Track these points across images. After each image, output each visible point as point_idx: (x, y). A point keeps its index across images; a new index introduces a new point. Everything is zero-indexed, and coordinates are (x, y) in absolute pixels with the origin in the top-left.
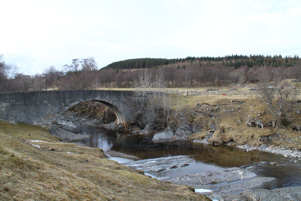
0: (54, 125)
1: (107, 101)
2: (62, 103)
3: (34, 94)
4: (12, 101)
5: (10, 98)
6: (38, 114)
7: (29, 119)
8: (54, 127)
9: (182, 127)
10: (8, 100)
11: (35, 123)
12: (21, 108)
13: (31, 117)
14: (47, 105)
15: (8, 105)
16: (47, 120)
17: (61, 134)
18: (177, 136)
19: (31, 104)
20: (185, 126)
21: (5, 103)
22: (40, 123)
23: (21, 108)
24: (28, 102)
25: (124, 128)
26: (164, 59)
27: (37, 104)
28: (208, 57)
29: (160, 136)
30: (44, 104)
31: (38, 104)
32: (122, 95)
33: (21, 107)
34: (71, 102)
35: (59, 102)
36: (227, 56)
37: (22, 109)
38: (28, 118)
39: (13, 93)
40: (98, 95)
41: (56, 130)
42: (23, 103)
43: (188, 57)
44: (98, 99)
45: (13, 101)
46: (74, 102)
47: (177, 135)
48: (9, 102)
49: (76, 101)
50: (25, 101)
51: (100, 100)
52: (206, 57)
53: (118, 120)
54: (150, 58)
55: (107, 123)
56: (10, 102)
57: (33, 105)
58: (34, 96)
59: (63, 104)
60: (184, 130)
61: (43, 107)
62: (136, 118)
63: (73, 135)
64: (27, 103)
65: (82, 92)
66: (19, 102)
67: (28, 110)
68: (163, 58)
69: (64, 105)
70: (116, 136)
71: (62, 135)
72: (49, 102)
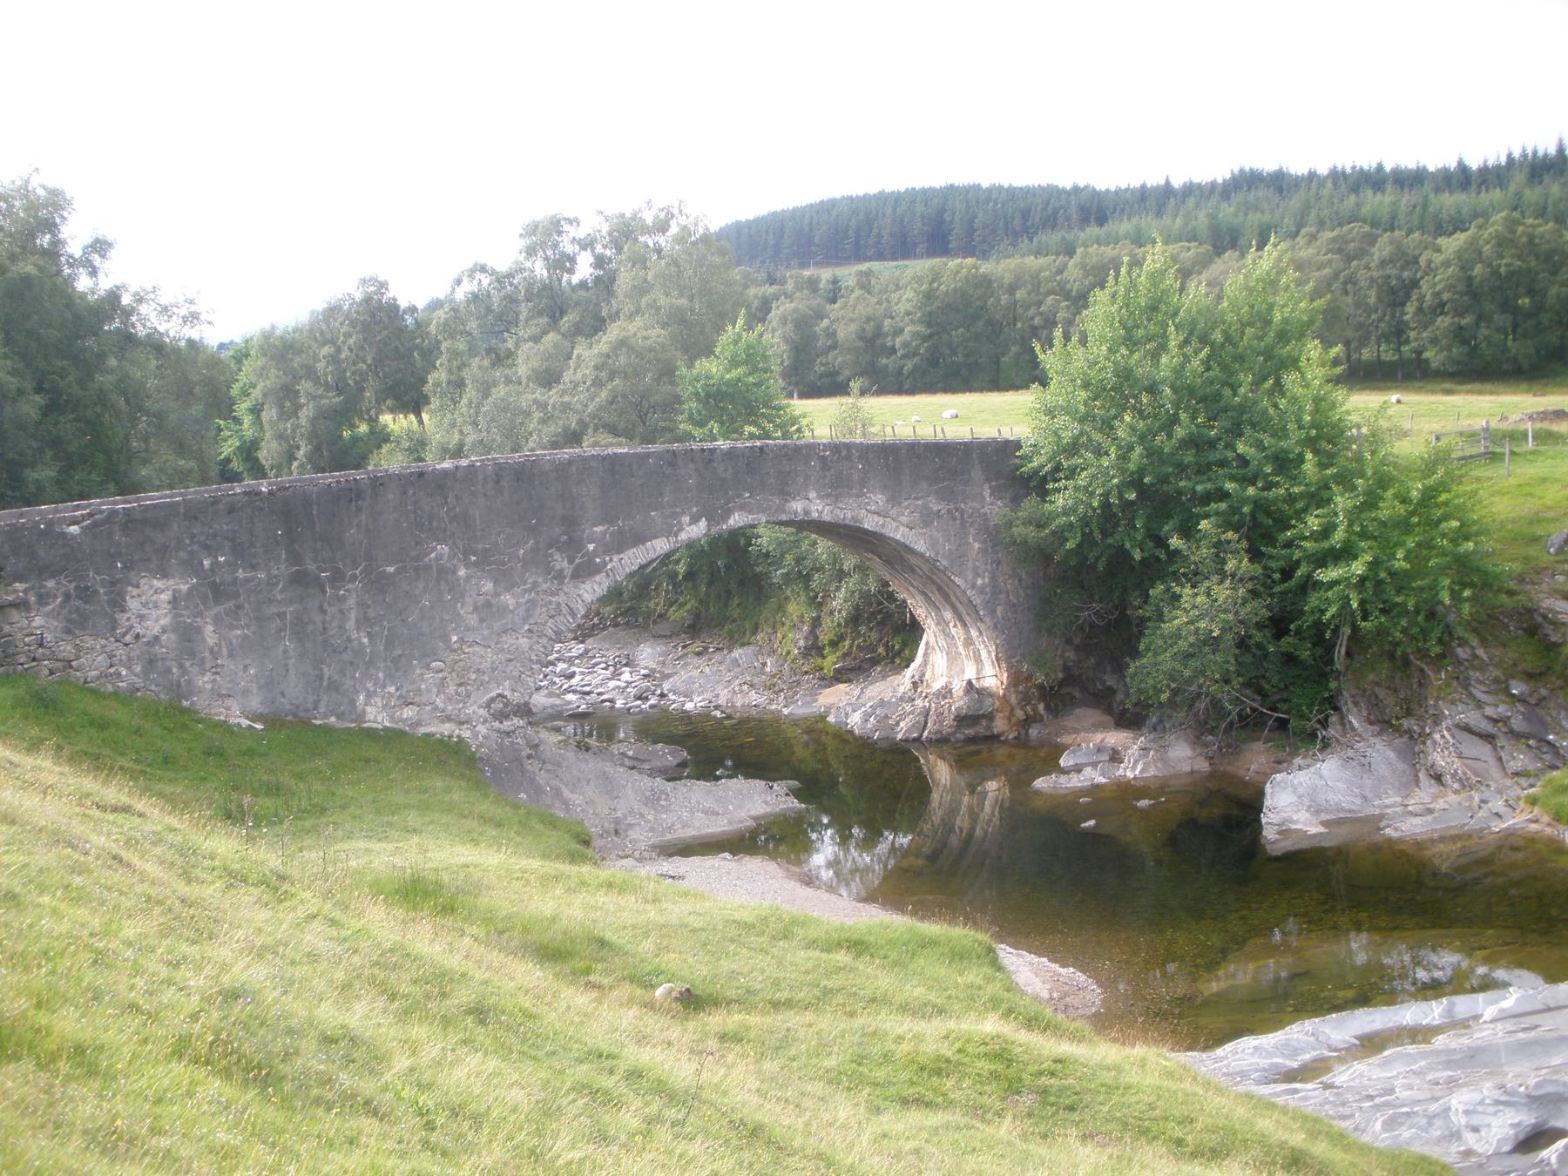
0: (507, 725)
1: (870, 523)
2: (557, 556)
3: (359, 496)
4: (206, 563)
5: (192, 536)
6: (389, 644)
7: (334, 686)
8: (508, 734)
9: (1471, 717)
10: (182, 554)
11: (376, 716)
12: (275, 609)
13: (342, 672)
14: (455, 572)
15: (184, 588)
16: (452, 689)
17: (566, 793)
18: (1435, 788)
19: (338, 577)
20: (1489, 711)
21: (165, 576)
22: (408, 712)
23: (275, 609)
24: (315, 560)
25: (990, 717)
26: (1076, 189)
27: (383, 575)
28: (1380, 168)
29: (1315, 788)
30: (428, 567)
31: (391, 569)
32: (977, 474)
33: (270, 601)
34: (621, 543)
35: (535, 550)
36: (1517, 154)
37: (282, 616)
38: (320, 678)
39: (215, 501)
40: (807, 477)
41: (529, 757)
42: (282, 569)
43: (1191, 183)
44: (807, 512)
45: (215, 564)
46: (639, 539)
47: (1438, 778)
48: (193, 567)
49: (656, 537)
50: (295, 558)
51: (827, 518)
52: (1366, 167)
53: (939, 661)
54: (977, 187)
55: (840, 677)
56: (197, 570)
57: (354, 578)
58: (359, 509)
59: (565, 564)
60: (1489, 738)
61: (425, 590)
62: (1077, 641)
63: (653, 800)
64: (311, 567)
65: (692, 466)
66: (253, 567)
67: (318, 618)
68: (1066, 183)
69: (568, 571)
70: (923, 788)
71: (577, 799)
72: (466, 553)
